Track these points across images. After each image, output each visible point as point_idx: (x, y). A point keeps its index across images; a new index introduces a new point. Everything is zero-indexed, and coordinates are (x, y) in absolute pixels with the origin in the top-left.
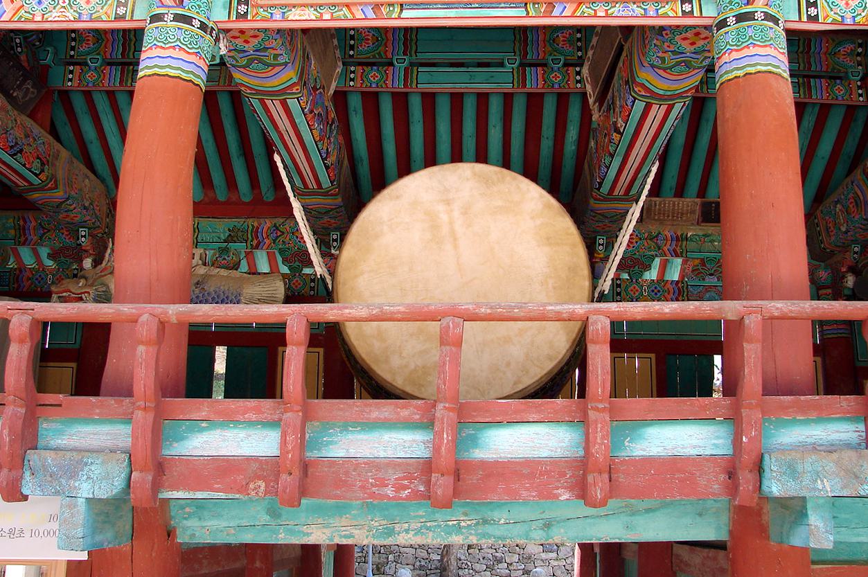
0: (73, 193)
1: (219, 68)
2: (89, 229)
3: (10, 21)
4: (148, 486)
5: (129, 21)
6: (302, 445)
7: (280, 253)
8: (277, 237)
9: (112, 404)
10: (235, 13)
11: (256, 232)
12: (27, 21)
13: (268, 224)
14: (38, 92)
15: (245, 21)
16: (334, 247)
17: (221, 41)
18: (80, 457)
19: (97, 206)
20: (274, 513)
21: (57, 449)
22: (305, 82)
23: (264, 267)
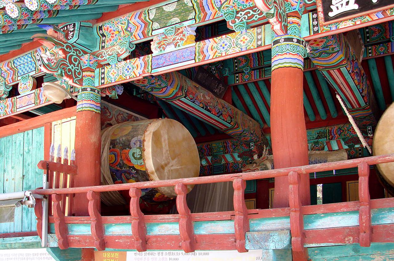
0: (245, 128)
1: (307, 60)
2: (254, 142)
3: (212, 59)
4: (299, 242)
5: (263, 46)
6: (370, 220)
7: (343, 140)
8: (341, 133)
9: (280, 211)
10: (312, 32)
11: (330, 132)
12: (219, 57)
14: (225, 88)
15: (318, 34)
16: (370, 133)
17: (307, 47)
18: (269, 233)
19: (257, 132)
20: (356, 250)
21: (258, 231)
22: (348, 58)
23: (335, 147)
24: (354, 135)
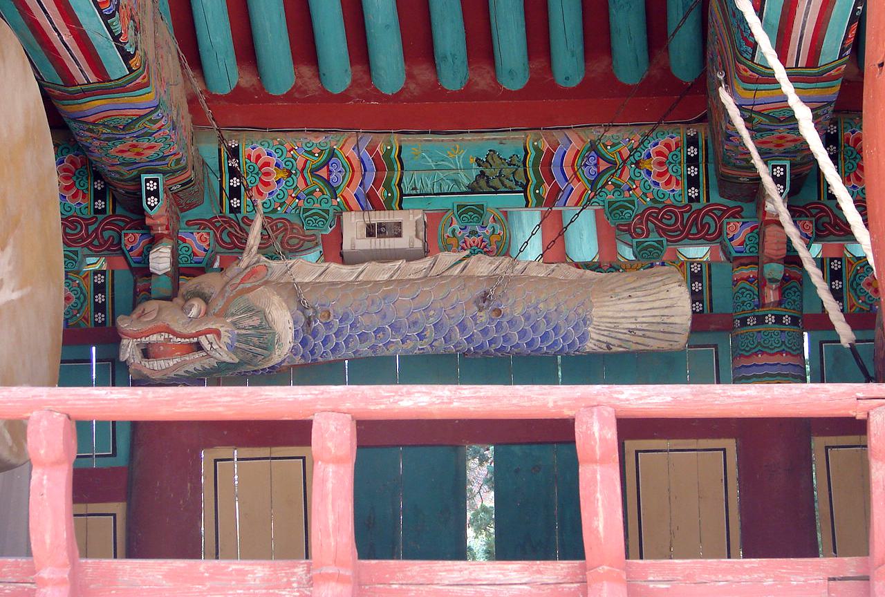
11: (545, 161)
13: (576, 145)
24: (667, 191)
